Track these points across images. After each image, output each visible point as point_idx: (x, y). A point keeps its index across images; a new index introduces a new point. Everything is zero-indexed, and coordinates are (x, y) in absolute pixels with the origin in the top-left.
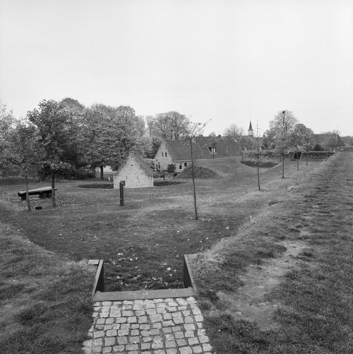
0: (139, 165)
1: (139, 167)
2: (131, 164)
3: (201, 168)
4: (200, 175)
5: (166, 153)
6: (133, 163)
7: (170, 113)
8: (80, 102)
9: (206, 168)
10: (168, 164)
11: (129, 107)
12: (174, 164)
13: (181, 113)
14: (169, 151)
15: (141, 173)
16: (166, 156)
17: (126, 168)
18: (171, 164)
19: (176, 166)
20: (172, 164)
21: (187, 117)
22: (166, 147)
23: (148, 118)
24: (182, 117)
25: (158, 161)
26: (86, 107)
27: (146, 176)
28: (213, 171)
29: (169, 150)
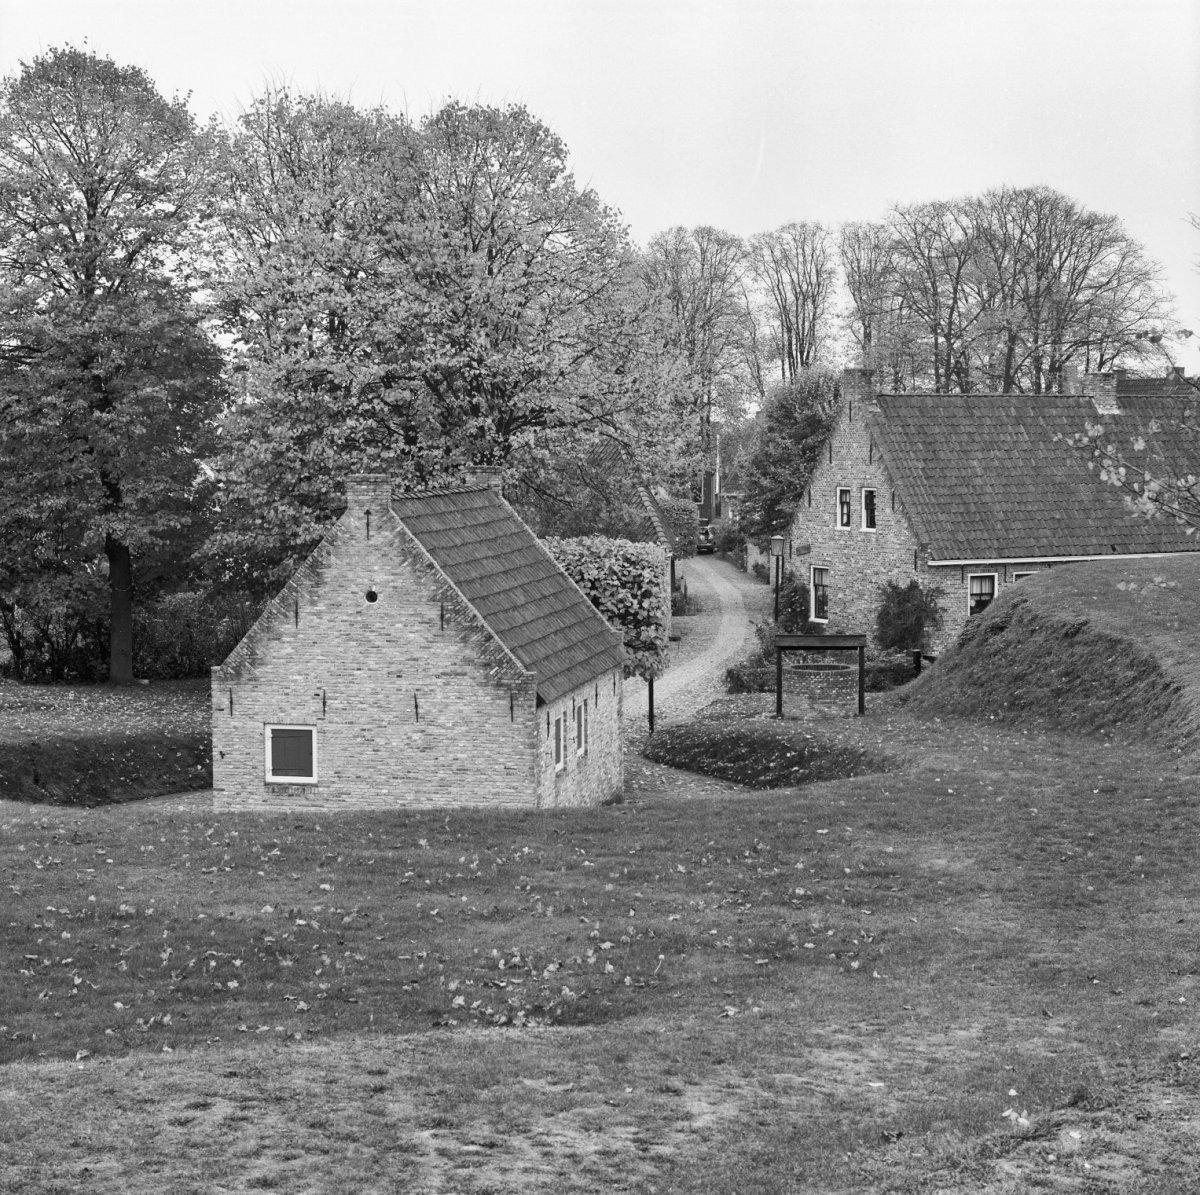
0: (433, 599)
1: (433, 613)
2: (363, 581)
3: (1072, 633)
4: (1058, 693)
5: (870, 496)
6: (380, 576)
7: (1005, 202)
8: (166, 90)
9: (1116, 635)
10: (883, 580)
11: (518, 115)
12: (924, 581)
13: (1087, 200)
14: (891, 480)
15: (445, 664)
16: (871, 523)
17: (319, 614)
18: (903, 585)
19: (941, 602)
20: (914, 586)
21: (1129, 235)
22: (873, 446)
23: (854, 238)
24: (1095, 231)
25: (814, 559)
26: (201, 122)
27: (484, 697)
28: (1167, 664)
29: (896, 474)
